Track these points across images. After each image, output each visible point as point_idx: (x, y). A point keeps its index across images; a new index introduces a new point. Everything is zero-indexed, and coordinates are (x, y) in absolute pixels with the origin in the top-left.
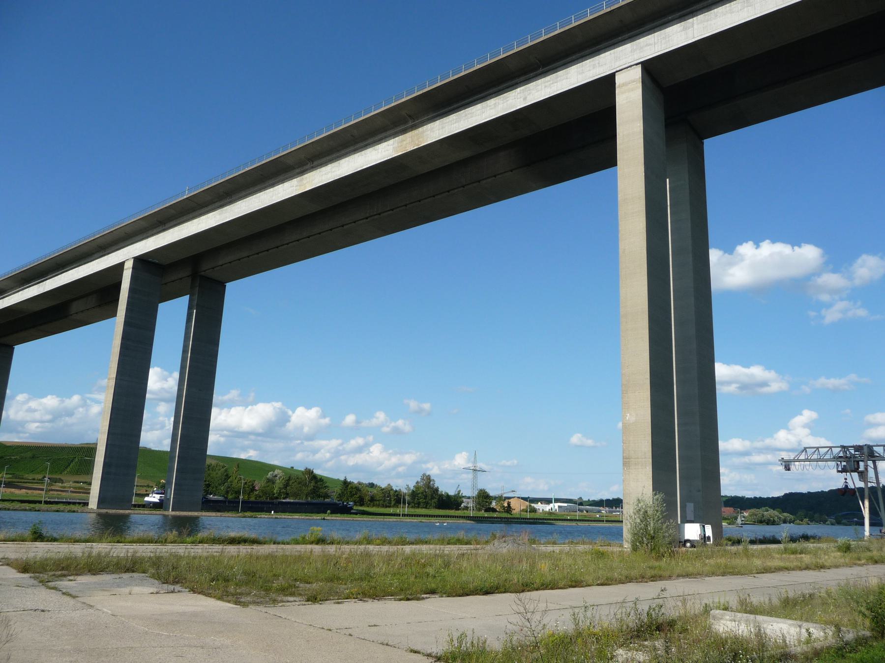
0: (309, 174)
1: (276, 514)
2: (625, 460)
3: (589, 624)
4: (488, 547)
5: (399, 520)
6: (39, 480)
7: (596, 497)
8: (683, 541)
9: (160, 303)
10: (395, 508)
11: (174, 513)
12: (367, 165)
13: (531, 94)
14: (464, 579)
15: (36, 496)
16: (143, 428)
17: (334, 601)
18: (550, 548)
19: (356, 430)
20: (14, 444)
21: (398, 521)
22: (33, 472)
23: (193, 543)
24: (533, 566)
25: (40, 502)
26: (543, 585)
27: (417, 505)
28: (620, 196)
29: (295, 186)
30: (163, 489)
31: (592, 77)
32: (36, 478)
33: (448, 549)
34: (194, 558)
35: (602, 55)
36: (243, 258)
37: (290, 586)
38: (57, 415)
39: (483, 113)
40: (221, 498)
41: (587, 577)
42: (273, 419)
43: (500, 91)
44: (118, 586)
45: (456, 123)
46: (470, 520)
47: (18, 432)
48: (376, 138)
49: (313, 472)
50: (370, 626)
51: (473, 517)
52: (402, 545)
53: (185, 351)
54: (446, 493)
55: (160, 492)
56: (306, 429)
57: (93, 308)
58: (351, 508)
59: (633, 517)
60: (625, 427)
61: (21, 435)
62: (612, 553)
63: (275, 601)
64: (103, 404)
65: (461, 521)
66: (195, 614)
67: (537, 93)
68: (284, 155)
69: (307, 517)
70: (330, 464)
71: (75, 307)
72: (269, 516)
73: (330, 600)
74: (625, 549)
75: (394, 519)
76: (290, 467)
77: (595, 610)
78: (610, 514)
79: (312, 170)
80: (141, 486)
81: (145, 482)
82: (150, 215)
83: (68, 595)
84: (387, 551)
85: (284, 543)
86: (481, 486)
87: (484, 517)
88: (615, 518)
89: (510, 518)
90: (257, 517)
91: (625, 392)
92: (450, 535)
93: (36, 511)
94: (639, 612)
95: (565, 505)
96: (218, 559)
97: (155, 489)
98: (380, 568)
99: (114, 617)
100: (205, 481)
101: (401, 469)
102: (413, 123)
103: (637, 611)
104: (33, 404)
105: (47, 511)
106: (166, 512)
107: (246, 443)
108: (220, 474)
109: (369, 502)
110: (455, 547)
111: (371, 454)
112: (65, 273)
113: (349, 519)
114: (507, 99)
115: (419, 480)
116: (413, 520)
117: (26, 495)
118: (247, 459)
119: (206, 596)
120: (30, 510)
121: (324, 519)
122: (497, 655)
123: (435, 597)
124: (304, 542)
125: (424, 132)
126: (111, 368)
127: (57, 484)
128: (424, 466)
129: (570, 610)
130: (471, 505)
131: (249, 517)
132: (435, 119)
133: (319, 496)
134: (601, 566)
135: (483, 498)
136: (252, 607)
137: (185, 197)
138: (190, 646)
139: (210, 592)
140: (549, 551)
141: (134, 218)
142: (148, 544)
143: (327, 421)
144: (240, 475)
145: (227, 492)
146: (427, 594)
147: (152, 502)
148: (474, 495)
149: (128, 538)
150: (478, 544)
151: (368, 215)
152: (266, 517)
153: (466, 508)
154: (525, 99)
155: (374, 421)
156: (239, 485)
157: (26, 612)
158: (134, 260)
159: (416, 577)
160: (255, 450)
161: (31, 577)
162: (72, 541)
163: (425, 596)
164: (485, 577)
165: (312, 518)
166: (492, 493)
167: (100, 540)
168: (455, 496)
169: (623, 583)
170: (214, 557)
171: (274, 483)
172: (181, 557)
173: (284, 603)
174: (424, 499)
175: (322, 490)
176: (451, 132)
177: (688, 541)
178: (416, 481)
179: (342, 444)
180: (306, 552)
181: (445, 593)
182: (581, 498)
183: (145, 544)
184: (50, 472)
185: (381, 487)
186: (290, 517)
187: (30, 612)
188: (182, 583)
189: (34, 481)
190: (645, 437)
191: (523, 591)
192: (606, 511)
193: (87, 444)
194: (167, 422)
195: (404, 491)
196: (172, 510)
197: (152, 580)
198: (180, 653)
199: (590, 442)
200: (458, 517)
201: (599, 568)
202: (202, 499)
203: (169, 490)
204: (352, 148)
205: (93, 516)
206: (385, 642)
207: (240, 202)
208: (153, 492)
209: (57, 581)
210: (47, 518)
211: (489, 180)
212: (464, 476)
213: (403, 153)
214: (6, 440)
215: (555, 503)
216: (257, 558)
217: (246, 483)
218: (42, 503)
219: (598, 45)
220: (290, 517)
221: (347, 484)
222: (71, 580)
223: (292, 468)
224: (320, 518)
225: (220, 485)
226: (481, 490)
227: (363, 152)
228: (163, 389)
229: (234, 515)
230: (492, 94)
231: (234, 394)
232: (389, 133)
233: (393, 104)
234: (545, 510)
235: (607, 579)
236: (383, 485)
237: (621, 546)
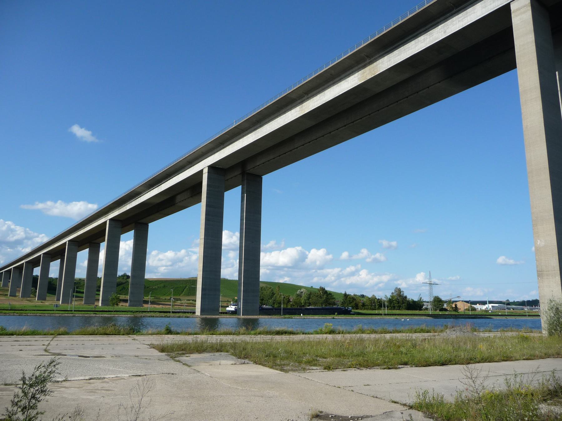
0: (306, 103)
1: (304, 316)
2: (539, 273)
3: (518, 387)
4: (442, 334)
5: (382, 318)
6: (169, 300)
7: (520, 299)
9: (121, 234)
10: (379, 310)
11: (243, 317)
12: (342, 92)
13: (449, 29)
14: (426, 355)
15: (167, 309)
16: (222, 267)
17: (342, 369)
18: (487, 335)
19: (349, 261)
20: (154, 279)
21: (381, 318)
22: (165, 295)
23: (255, 334)
24: (475, 347)
25: (170, 312)
26: (482, 359)
28: (521, 89)
29: (298, 111)
30: (236, 303)
31: (493, 9)
32: (167, 299)
33: (415, 336)
34: (256, 343)
36: (271, 160)
37: (314, 360)
38: (174, 262)
39: (416, 46)
40: (270, 307)
41: (515, 355)
42: (297, 257)
43: (426, 30)
44: (213, 360)
45: (398, 56)
46: (430, 317)
47: (155, 273)
48: (348, 73)
49: (324, 289)
50: (364, 385)
51: (432, 315)
52: (384, 334)
53: (242, 219)
54: (412, 299)
55: (235, 304)
56: (318, 263)
57: (188, 198)
58: (350, 311)
59: (548, 312)
60: (537, 249)
61: (157, 274)
62: (534, 337)
63: (304, 369)
64: (198, 254)
65: (424, 318)
66: (257, 377)
67: (453, 27)
69: (323, 317)
70: (335, 284)
71: (179, 198)
72: (300, 317)
73: (339, 368)
74: (544, 335)
75: (379, 317)
76: (310, 287)
77: (522, 377)
78: (531, 311)
79: (308, 100)
80: (224, 301)
81: (226, 299)
82: (215, 139)
83: (186, 365)
84: (374, 338)
85: (309, 334)
86: (435, 294)
87: (439, 315)
88: (536, 313)
89: (458, 315)
90: (292, 318)
91: (534, 225)
92: (416, 327)
93: (168, 317)
94: (556, 378)
95: (497, 305)
96: (269, 343)
97: (232, 303)
98: (371, 348)
99: (211, 378)
100: (260, 297)
101: (381, 285)
102: (369, 61)
103: (555, 377)
104: (161, 256)
105: (174, 317)
106: (239, 316)
107: (282, 273)
108: (268, 293)
110: (420, 334)
111: (360, 276)
112: (171, 180)
113: (350, 318)
116: (391, 318)
117: (162, 308)
118: (284, 283)
119: (263, 366)
120: (165, 317)
121: (334, 318)
122: (451, 406)
123: (407, 367)
124: (321, 333)
125: (377, 65)
126: (201, 232)
127: (178, 301)
128: (395, 282)
129: (504, 377)
130: (429, 307)
131: (288, 318)
133: (330, 304)
134: (525, 346)
135: (438, 302)
136: (291, 373)
138: (255, 396)
139: (266, 364)
140: (486, 336)
141: (238, 123)
142: (229, 335)
143: (330, 256)
144: (280, 293)
145: (274, 303)
146: (402, 365)
147: (231, 310)
148: (431, 300)
149: (218, 332)
150: (436, 332)
151: (345, 124)
153: (426, 309)
154: (445, 32)
155: (361, 256)
156: (281, 298)
157: (164, 374)
159: (394, 354)
160: (288, 277)
161: (166, 355)
162: (188, 334)
163: (400, 366)
164: (440, 354)
166: (443, 299)
167: (202, 333)
168: (418, 301)
169: (543, 358)
170: (267, 342)
171: (301, 297)
172: (248, 343)
173: (310, 371)
174: (398, 304)
175: (331, 300)
176: (395, 63)
178: (392, 292)
179: (341, 271)
180: (322, 339)
181: (414, 365)
182: (508, 300)
183: (227, 335)
184: (174, 295)
185: (368, 297)
187: (166, 374)
188: (249, 358)
189: (166, 300)
190: (553, 256)
191: (469, 363)
192: (528, 309)
193: (192, 278)
194: (235, 262)
195: (384, 299)
196: (243, 315)
197: (232, 356)
198: (249, 400)
199: (512, 262)
200: (421, 315)
201: (524, 348)
202: (259, 308)
203: (240, 303)
204: (331, 82)
206: (375, 396)
207: (266, 125)
208: (231, 305)
209: (179, 357)
210: (173, 321)
211: (424, 91)
212: (424, 288)
213: (365, 81)
214: (149, 278)
215: (489, 304)
216: (293, 343)
217: (284, 298)
219: (461, 6)
220: (312, 317)
221: (347, 296)
222: (187, 357)
223: (312, 287)
224: (331, 317)
225: (269, 299)
226: (436, 297)
227: (339, 84)
228: (231, 243)
229: (279, 317)
231: (272, 243)
232: (354, 69)
233: (355, 50)
234: (482, 309)
235: (530, 356)
236: (370, 296)
237: (541, 332)
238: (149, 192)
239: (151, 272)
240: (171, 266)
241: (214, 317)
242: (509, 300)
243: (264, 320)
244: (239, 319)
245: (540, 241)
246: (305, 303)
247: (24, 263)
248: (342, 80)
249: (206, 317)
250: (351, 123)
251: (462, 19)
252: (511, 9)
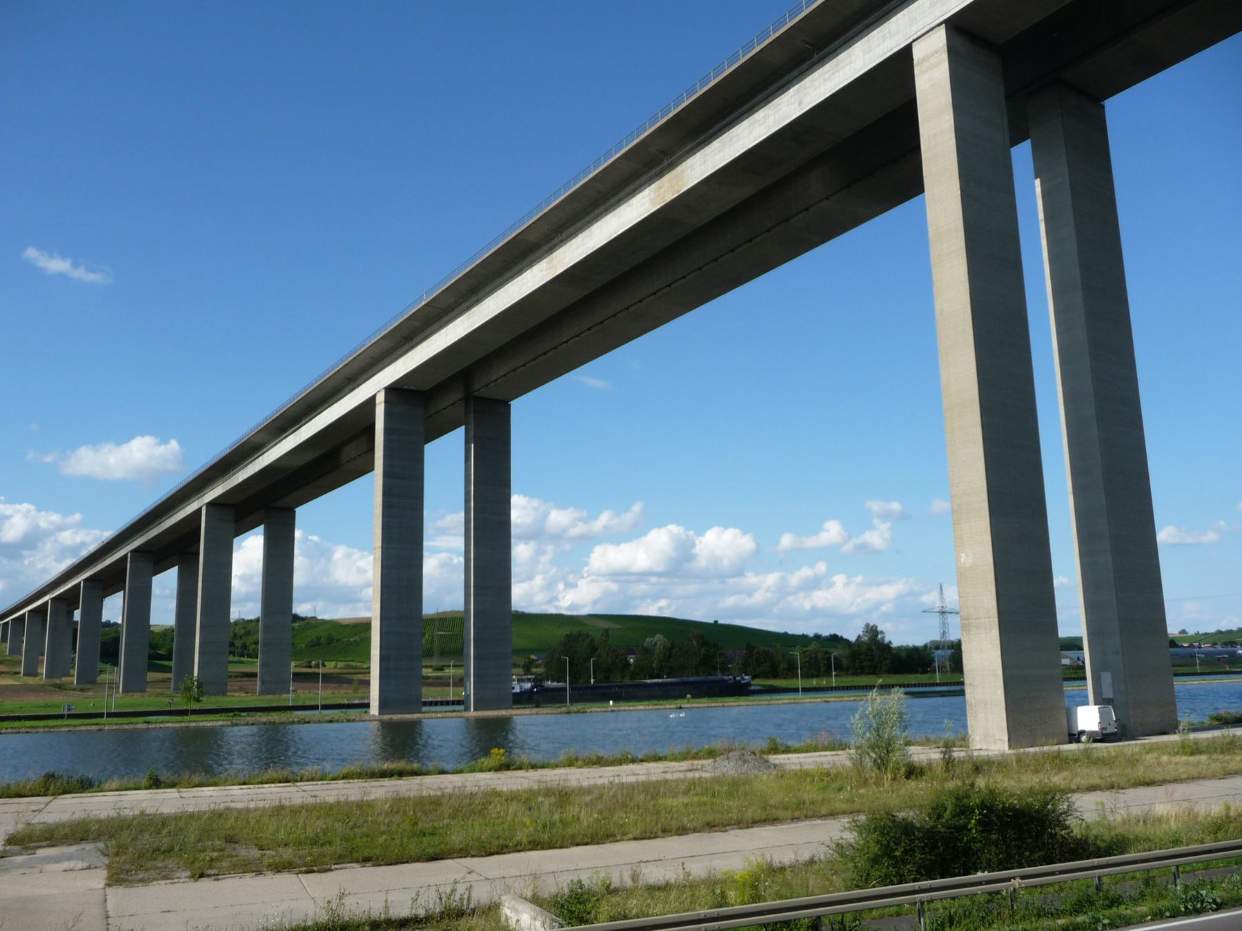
2: (963, 622)
8: (1077, 733)
11: (482, 714)
16: (513, 580)
27: (859, 671)
28: (931, 230)
35: (893, 20)
43: (768, 96)
45: (719, 152)
53: (467, 501)
57: (365, 453)
68: (522, 231)
90: (586, 712)
93: (305, 723)
109: (786, 671)
114: (779, 107)
115: (861, 634)
132: (695, 151)
137: (423, 303)
141: (431, 295)
151: (656, 289)
154: (800, 103)
158: (385, 391)
165: (663, 707)
177: (1082, 732)
196: (475, 710)
203: (468, 683)
205: (376, 725)
211: (800, 216)
218: (318, 709)
220: (631, 708)
224: (675, 706)
230: (760, 102)
233: (635, 142)
238: (278, 445)
241: (409, 716)
242: (1187, 631)
244: (468, 719)
245: (965, 555)
247: (48, 601)
248: (621, 202)
249: (391, 719)
250: (666, 287)
251: (830, 76)
252: (914, 57)
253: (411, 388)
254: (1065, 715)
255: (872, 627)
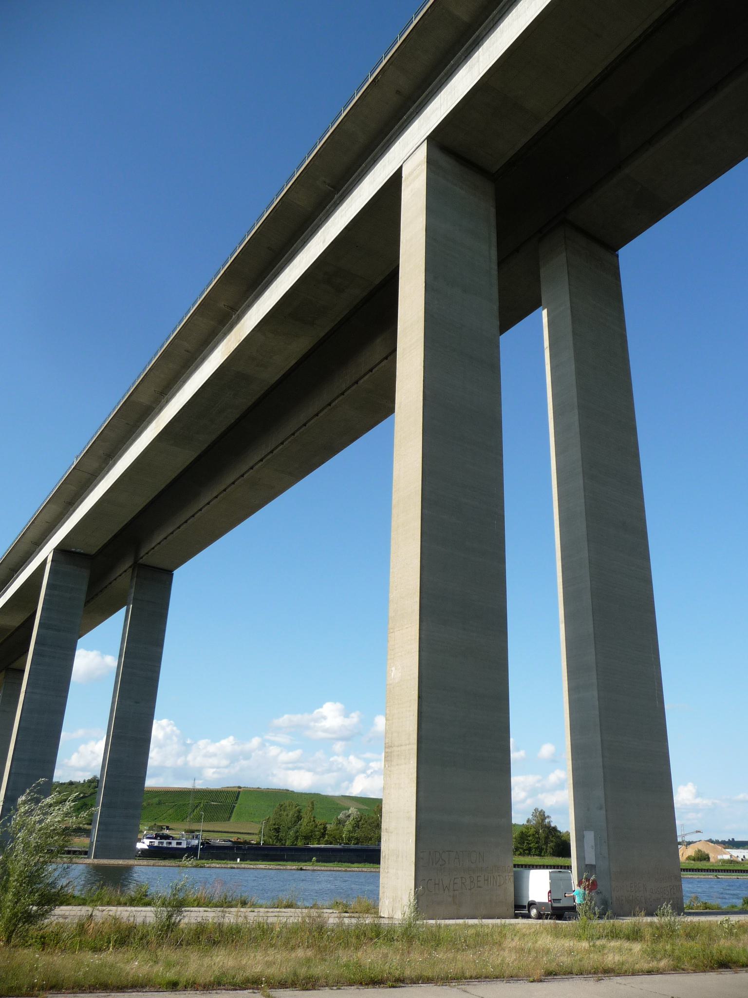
2: (387, 750)
11: (96, 861)
27: (527, 852)
38: (233, 758)
115: (531, 817)
121: (301, 869)
145: (297, 838)
152: (217, 866)
177: (532, 904)
178: (527, 819)
186: (252, 866)
220: (252, 866)
239: (154, 775)
240: (226, 767)
241: (120, 862)
243: (143, 869)
246: (350, 839)
251: (346, 212)
253: (78, 550)
254: (512, 879)
255: (540, 812)
